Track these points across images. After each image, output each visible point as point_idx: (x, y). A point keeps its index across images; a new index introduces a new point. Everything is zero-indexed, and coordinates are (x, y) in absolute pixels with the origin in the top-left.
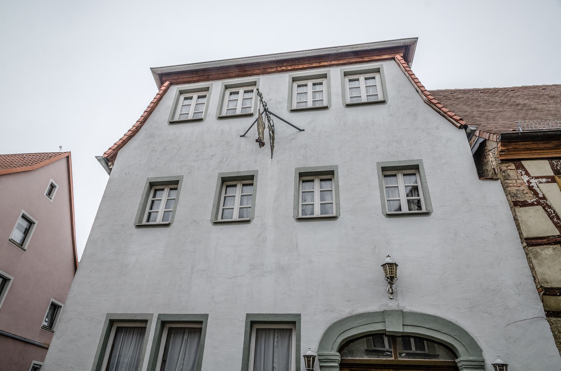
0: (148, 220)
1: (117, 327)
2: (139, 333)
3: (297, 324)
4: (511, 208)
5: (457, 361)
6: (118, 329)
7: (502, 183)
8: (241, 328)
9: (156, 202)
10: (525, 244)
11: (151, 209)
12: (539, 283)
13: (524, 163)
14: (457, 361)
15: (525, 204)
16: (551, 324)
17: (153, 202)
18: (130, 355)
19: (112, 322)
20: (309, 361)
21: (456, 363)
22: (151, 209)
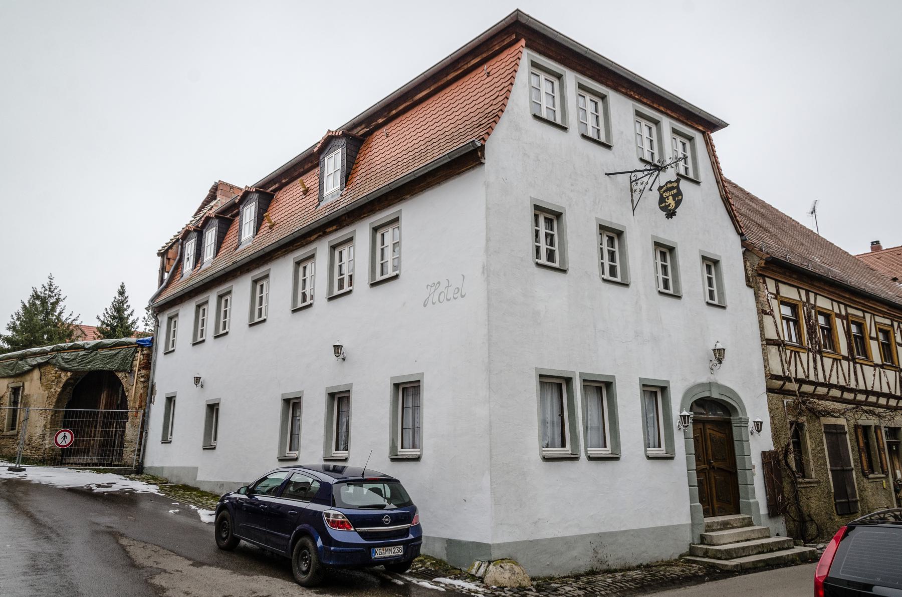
0: (382, 274)
1: (403, 388)
2: (400, 575)
3: (350, 392)
4: (758, 313)
5: (731, 418)
6: (403, 389)
7: (755, 291)
8: (387, 392)
9: (385, 249)
10: (764, 342)
11: (382, 259)
12: (769, 370)
13: (767, 279)
14: (731, 418)
15: (766, 314)
16: (768, 395)
17: (382, 249)
18: (888, 310)
19: (397, 386)
20: (758, 425)
21: (731, 419)
22: (382, 259)
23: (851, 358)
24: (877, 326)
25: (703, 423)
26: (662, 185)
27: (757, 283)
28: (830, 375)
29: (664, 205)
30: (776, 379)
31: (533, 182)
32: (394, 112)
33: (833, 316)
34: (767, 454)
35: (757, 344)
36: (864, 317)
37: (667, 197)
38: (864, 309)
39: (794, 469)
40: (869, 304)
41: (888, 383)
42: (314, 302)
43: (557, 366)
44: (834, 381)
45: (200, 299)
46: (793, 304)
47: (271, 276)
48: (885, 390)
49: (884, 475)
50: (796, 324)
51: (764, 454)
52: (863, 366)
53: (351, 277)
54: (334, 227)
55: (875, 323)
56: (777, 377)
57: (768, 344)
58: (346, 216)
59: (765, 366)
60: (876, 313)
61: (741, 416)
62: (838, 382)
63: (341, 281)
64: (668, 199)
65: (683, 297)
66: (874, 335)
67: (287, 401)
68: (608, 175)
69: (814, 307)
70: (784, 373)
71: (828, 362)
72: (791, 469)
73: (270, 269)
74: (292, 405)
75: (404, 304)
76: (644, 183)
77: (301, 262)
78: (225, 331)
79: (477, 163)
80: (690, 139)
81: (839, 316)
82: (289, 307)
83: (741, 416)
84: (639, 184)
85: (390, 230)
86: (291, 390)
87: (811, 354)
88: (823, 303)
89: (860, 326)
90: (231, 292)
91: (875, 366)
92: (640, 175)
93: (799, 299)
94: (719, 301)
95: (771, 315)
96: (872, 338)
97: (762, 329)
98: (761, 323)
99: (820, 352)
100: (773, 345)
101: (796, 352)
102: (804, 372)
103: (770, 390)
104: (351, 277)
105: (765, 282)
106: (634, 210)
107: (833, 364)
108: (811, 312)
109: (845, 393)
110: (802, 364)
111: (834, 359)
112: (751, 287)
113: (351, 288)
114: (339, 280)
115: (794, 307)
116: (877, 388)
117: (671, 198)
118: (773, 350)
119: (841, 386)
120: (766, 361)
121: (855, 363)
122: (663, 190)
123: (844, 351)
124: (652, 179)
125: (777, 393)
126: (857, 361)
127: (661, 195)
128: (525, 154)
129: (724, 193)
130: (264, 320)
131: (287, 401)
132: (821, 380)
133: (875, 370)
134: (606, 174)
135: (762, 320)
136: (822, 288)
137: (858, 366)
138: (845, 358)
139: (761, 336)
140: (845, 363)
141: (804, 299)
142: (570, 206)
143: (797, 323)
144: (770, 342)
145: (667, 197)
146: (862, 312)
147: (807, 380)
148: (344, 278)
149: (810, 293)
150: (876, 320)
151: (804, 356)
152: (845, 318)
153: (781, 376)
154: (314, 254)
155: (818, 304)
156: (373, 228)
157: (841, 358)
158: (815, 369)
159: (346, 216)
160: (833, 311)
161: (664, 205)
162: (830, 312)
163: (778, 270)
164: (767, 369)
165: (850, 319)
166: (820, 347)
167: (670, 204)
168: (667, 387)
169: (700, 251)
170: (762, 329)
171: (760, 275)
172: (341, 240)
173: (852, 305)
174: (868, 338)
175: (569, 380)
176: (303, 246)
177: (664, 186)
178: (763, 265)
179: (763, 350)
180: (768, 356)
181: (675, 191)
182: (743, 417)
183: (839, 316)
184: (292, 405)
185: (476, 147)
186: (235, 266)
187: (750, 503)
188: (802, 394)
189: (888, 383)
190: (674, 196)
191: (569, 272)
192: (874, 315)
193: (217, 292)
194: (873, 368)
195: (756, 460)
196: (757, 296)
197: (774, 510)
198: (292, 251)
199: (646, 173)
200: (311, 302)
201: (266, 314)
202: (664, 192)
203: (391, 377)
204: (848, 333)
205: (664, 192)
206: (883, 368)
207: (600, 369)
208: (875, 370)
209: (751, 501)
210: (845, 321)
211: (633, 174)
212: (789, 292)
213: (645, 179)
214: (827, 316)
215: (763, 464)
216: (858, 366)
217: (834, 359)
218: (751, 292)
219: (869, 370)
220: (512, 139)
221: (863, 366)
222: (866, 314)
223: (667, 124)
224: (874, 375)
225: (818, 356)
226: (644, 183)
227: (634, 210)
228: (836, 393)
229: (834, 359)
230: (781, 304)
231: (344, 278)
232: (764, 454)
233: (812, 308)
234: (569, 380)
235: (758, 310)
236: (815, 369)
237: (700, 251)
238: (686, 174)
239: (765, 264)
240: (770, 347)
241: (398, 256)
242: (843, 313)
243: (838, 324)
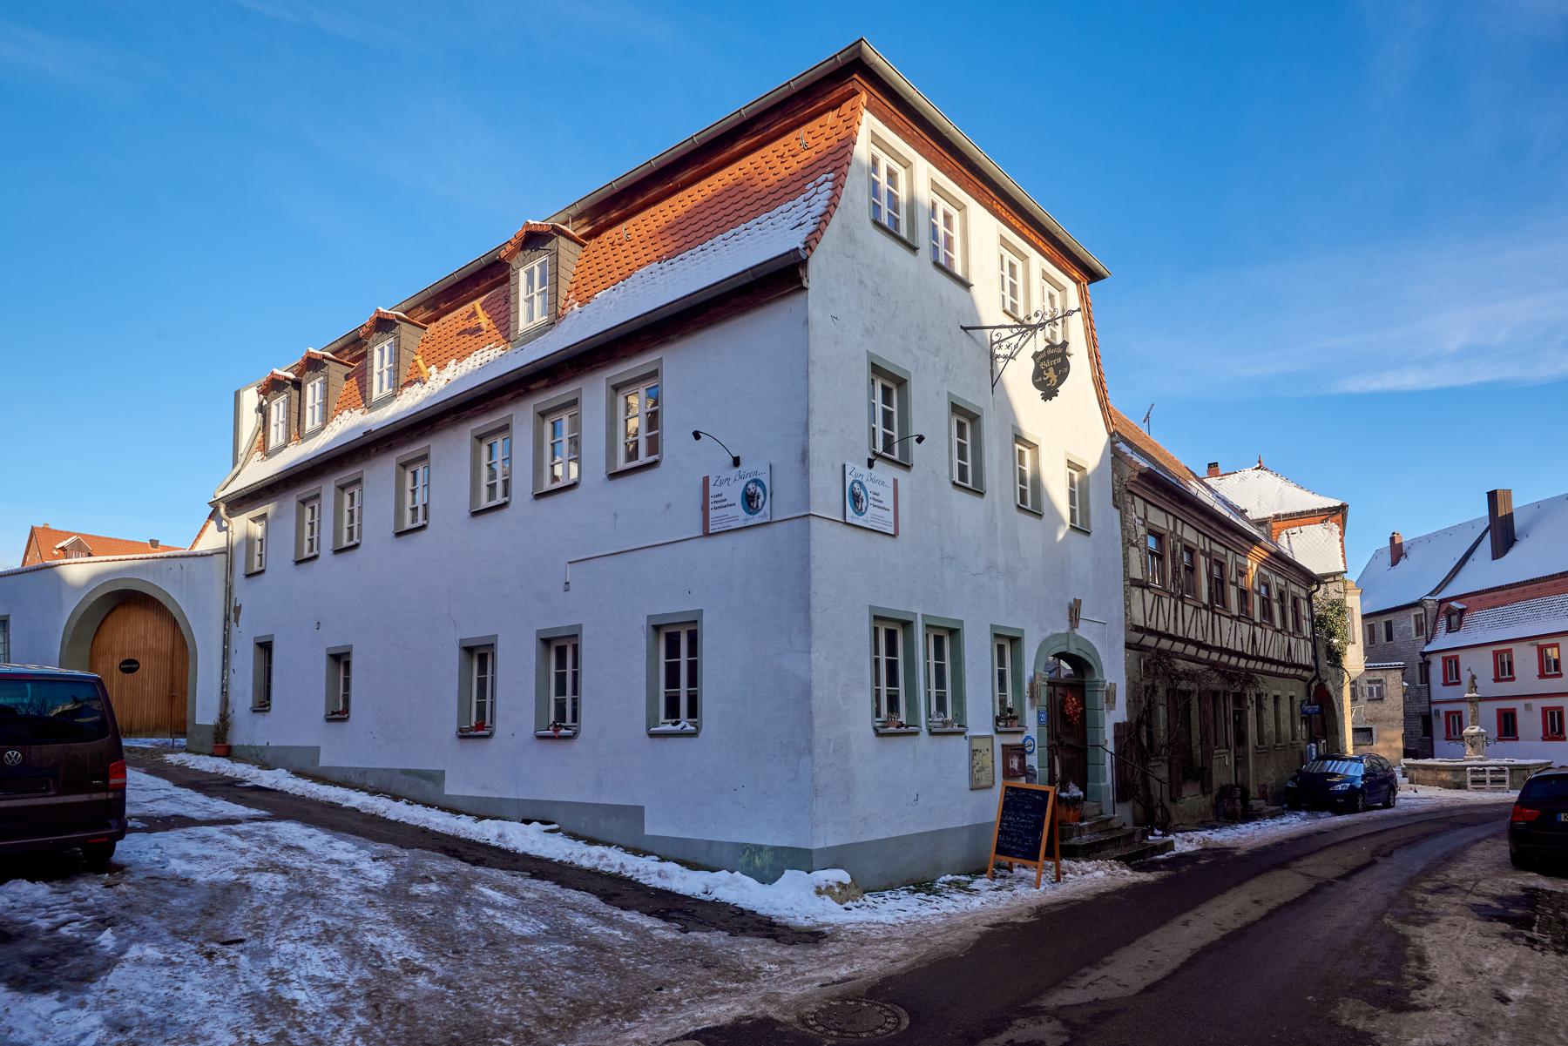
10: (1128, 583)
15: (1133, 545)
21: (1084, 682)
23: (1210, 608)
24: (1239, 568)
25: (1054, 687)
26: (1039, 350)
27: (1124, 503)
28: (1189, 628)
29: (1040, 379)
30: (1136, 631)
31: (871, 328)
32: (640, 201)
33: (1198, 552)
34: (1121, 725)
35: (1119, 583)
36: (1226, 556)
37: (1046, 369)
38: (1228, 545)
39: (1145, 745)
40: (1235, 540)
41: (1242, 639)
42: (510, 499)
43: (896, 605)
44: (1192, 636)
45: (307, 490)
46: (1160, 534)
47: (515, 426)
48: (1239, 649)
49: (1227, 750)
50: (1161, 560)
51: (1117, 725)
52: (1222, 617)
53: (506, 483)
54: (544, 382)
55: (1236, 563)
56: (1138, 629)
57: (1131, 585)
58: (566, 364)
59: (1126, 615)
60: (1238, 551)
61: (1097, 677)
62: (1196, 637)
63: (492, 487)
64: (1047, 372)
65: (1045, 516)
66: (1233, 579)
67: (468, 650)
68: (965, 329)
69: (1181, 539)
70: (1145, 623)
71: (1189, 610)
72: (1141, 744)
73: (362, 471)
74: (479, 655)
75: (669, 506)
76: (1013, 346)
77: (547, 414)
78: (312, 554)
79: (796, 287)
80: (1062, 289)
81: (1203, 552)
82: (390, 528)
83: (1097, 677)
84: (1004, 347)
85: (500, 441)
86: (475, 632)
87: (1173, 600)
88: (1190, 535)
89: (1221, 565)
90: (508, 428)
91: (1232, 617)
92: (1006, 333)
93: (1166, 527)
94: (1081, 524)
95: (1137, 547)
96: (1231, 583)
97: (1126, 565)
98: (1126, 557)
99: (1182, 598)
100: (1137, 586)
101: (1159, 596)
102: (1165, 622)
103: (1128, 646)
104: (506, 483)
105: (1133, 501)
106: (993, 386)
107: (1193, 614)
108: (1177, 545)
109: (1201, 651)
110: (1163, 612)
111: (1196, 608)
112: (1117, 508)
113: (506, 499)
114: (647, 437)
115: (1159, 537)
116: (1231, 646)
117: (1051, 369)
118: (1137, 592)
119: (1198, 642)
120: (1128, 606)
121: (1214, 613)
122: (1040, 358)
123: (1205, 600)
124: (1023, 340)
125: (1133, 649)
126: (1217, 610)
127: (1037, 366)
128: (861, 282)
129: (1098, 374)
130: (356, 546)
131: (468, 650)
132: (1180, 634)
133: (1231, 622)
134: (962, 327)
135: (1127, 553)
136: (1190, 515)
137: (1216, 617)
138: (1206, 607)
139: (1124, 574)
140: (1204, 612)
141: (1171, 528)
142: (917, 370)
143: (1160, 557)
144: (1136, 583)
145: (1046, 369)
146: (1224, 549)
147: (1166, 633)
148: (495, 483)
149: (1178, 520)
150: (1238, 560)
151: (1166, 601)
152: (1208, 555)
153: (1142, 627)
154: (508, 424)
155: (1185, 536)
156: (613, 387)
157: (1202, 606)
158: (1176, 619)
159: (566, 364)
160: (1198, 546)
161: (1040, 379)
162: (1195, 547)
163: (1151, 488)
164: (1129, 618)
165: (1214, 557)
166: (1182, 591)
167: (1050, 379)
168: (1020, 638)
169: (1066, 453)
170: (1126, 565)
171: (1130, 492)
172: (555, 404)
173: (1218, 540)
174: (1228, 582)
175: (907, 625)
176: (487, 411)
177: (1042, 352)
178: (1135, 479)
179: (1125, 592)
180: (1132, 601)
181: (1059, 360)
182: (1101, 679)
183: (1203, 552)
184: (479, 655)
185: (799, 260)
186: (369, 439)
187: (1100, 786)
188: (1160, 651)
189: (1242, 639)
190: (1057, 368)
191: (914, 469)
192: (1236, 553)
193: (472, 430)
194: (1229, 620)
195: (1109, 735)
196: (1123, 521)
197: (1123, 791)
198: (468, 419)
199: (1015, 330)
200: (425, 522)
201: (359, 537)
202: (1041, 361)
203: (648, 617)
204: (1210, 575)
205: (1041, 361)
206: (1239, 621)
207: (949, 612)
208: (1231, 622)
209: (1102, 784)
210: (1208, 560)
211: (997, 331)
212: (1158, 519)
213: (1014, 340)
214: (1190, 551)
215: (1115, 737)
216: (1216, 617)
217: (1196, 608)
218: (1116, 513)
219: (1226, 622)
220: (844, 254)
221: (1222, 617)
222: (1228, 551)
223: (1038, 262)
224: (1230, 629)
225: (1180, 603)
226: (1013, 346)
227: (993, 386)
228: (1191, 650)
229: (1195, 607)
230: (1149, 534)
231: (495, 483)
232: (1117, 725)
233: (1178, 540)
234: (907, 625)
235: (1123, 539)
236: (1176, 619)
237: (1066, 453)
238: (1052, 338)
239: (1138, 477)
240: (1133, 589)
241: (576, 456)
242: (1208, 549)
243: (1202, 562)
